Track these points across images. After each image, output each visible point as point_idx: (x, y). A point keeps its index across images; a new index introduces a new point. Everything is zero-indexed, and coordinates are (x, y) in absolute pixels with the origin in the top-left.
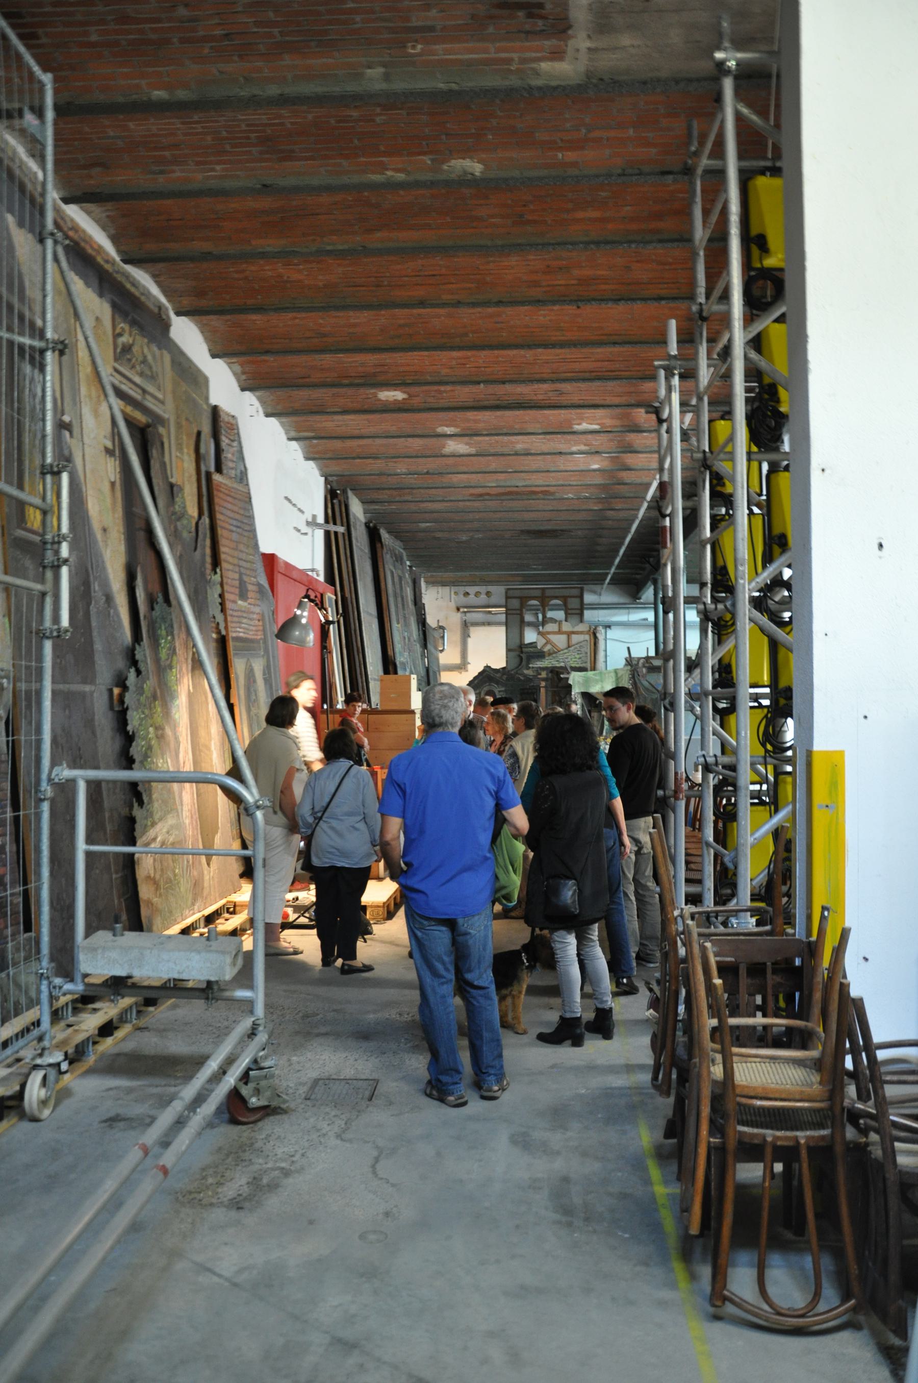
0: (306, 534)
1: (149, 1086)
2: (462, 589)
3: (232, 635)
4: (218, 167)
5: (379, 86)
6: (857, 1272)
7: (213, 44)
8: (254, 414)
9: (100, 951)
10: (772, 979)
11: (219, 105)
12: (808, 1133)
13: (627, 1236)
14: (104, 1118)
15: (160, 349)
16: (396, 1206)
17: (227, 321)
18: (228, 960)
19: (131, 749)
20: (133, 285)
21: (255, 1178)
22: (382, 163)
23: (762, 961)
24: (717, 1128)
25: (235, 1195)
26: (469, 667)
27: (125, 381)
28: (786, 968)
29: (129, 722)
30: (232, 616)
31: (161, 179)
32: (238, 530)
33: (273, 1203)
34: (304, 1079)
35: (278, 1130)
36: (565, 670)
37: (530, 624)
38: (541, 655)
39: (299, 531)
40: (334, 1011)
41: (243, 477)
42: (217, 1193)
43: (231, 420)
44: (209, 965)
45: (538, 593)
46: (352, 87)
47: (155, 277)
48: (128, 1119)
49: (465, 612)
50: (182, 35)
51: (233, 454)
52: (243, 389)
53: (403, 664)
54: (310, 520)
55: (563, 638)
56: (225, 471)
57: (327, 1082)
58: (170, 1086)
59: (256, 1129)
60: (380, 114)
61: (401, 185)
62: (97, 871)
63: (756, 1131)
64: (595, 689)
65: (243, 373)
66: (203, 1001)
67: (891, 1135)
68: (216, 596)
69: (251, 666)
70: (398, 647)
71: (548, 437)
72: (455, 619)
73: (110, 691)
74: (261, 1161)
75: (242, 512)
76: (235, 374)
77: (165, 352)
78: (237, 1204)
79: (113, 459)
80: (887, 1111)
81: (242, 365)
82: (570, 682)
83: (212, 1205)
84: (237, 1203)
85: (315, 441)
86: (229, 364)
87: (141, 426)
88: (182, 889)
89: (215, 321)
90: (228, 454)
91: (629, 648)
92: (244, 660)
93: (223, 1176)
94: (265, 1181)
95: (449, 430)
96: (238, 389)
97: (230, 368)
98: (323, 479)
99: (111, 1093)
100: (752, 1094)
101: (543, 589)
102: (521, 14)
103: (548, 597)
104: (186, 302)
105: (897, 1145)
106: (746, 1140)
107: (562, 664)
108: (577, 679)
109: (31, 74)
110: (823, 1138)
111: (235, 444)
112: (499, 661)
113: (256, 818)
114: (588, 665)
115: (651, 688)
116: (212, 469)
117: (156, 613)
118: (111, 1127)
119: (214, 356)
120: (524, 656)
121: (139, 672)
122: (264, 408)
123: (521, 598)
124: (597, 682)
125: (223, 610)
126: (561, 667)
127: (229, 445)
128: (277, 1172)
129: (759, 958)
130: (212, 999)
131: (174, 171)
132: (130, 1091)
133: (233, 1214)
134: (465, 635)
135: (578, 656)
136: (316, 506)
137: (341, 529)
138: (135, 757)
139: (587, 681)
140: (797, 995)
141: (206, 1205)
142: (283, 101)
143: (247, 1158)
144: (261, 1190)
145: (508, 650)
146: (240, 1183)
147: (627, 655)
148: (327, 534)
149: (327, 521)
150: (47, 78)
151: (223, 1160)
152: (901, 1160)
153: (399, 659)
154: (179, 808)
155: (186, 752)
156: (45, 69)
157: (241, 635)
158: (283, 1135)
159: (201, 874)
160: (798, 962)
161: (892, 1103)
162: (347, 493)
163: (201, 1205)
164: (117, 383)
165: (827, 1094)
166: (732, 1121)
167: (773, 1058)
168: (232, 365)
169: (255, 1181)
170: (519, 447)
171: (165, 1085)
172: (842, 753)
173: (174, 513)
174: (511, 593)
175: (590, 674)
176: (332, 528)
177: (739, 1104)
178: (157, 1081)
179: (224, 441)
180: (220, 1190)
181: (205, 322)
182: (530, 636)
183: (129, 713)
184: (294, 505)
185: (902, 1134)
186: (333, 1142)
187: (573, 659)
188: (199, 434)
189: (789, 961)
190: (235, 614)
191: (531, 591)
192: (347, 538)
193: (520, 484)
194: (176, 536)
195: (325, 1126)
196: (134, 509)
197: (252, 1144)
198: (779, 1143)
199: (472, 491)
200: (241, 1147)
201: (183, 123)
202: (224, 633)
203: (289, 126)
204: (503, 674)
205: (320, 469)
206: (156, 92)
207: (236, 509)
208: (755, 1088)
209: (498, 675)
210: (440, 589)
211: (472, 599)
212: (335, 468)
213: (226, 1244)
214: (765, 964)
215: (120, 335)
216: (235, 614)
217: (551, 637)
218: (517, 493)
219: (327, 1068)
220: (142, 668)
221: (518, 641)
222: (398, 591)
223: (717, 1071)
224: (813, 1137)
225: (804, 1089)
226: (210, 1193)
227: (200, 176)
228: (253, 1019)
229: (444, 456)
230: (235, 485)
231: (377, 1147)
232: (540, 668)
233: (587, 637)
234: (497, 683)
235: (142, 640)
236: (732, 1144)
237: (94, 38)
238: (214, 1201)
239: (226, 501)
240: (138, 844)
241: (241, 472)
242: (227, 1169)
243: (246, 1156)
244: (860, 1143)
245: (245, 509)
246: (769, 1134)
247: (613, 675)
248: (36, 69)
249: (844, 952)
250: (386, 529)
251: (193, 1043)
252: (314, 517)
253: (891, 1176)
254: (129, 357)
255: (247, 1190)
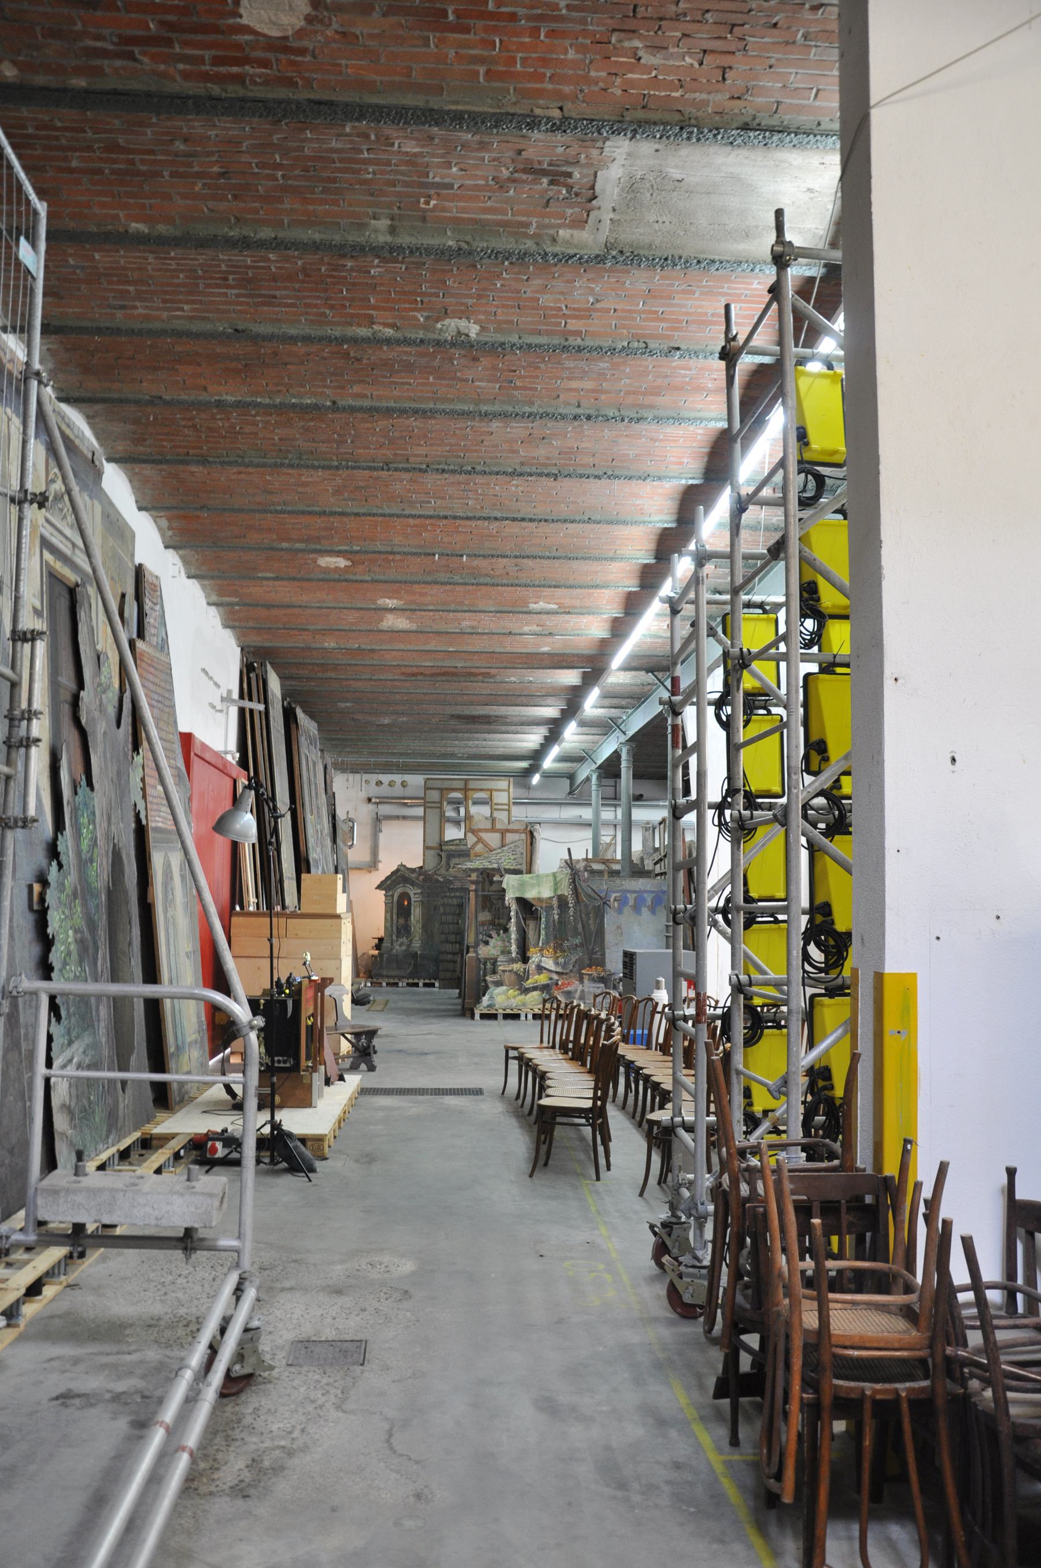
0: (221, 711)
1: (101, 1353)
2: (374, 778)
3: (152, 825)
4: (186, 307)
5: (384, 238)
6: (963, 1539)
7: (208, 181)
8: (176, 574)
9: (62, 1194)
10: (846, 1218)
11: (202, 243)
12: (908, 1385)
13: (692, 1510)
14: (54, 1395)
15: (91, 498)
16: (427, 1486)
17: (161, 470)
18: (217, 1203)
19: (51, 955)
20: (68, 426)
21: (253, 1460)
22: (371, 316)
23: (836, 1199)
24: (808, 1384)
25: (236, 1482)
26: (380, 865)
27: (55, 533)
28: (856, 1204)
29: (49, 923)
30: (151, 803)
31: (119, 314)
32: (160, 705)
33: (282, 1487)
34: (280, 1342)
35: (266, 1403)
36: (500, 872)
37: (449, 820)
38: (465, 854)
39: (214, 707)
40: (294, 1261)
41: (164, 646)
42: (213, 1480)
43: (155, 581)
44: (193, 1209)
45: (460, 785)
46: (353, 238)
47: (90, 418)
48: (84, 1395)
49: (377, 803)
50: (174, 169)
51: (155, 620)
52: (166, 547)
53: (316, 861)
54: (225, 695)
55: (497, 836)
56: (147, 639)
57: (307, 1344)
58: (124, 1353)
59: (240, 1402)
60: (378, 266)
61: (388, 341)
62: (11, 1098)
63: (852, 1384)
64: (530, 895)
65: (170, 528)
66: (180, 1251)
67: (1003, 1384)
68: (138, 780)
69: (169, 860)
70: (311, 842)
71: (498, 615)
72: (364, 813)
73: (30, 888)
74: (254, 1439)
75: (163, 684)
76: (160, 529)
77: (96, 503)
78: (241, 1491)
79: (40, 621)
80: (998, 1358)
81: (169, 519)
82: (504, 886)
83: (211, 1493)
84: (241, 1490)
85: (237, 608)
86: (155, 519)
87: (72, 585)
88: (97, 1119)
89: (148, 470)
90: (150, 620)
91: (569, 850)
92: (163, 854)
93: (215, 1460)
94: (267, 1463)
95: (390, 603)
96: (162, 546)
97: (155, 522)
98: (239, 649)
99: (54, 1364)
100: (847, 1344)
101: (466, 780)
102: (545, 181)
103: (472, 790)
104: (121, 447)
105: (1010, 1395)
106: (843, 1395)
107: (495, 866)
108: (511, 882)
109: (28, 202)
110: (922, 1390)
111: (158, 608)
112: (414, 860)
113: (249, 1039)
114: (524, 868)
115: (593, 894)
116: (135, 636)
117: (79, 799)
118: (65, 1405)
119: (140, 509)
120: (443, 854)
121: (60, 866)
122: (185, 569)
123: (441, 790)
124: (533, 886)
125: (144, 797)
126: (493, 869)
127: (152, 609)
128: (278, 1452)
129: (833, 1196)
130: (192, 1249)
131: (136, 308)
132: (76, 1361)
133: (240, 1503)
134: (376, 831)
135: (512, 857)
136: (232, 682)
137: (261, 707)
138: (54, 964)
139: (522, 885)
140: (868, 1235)
141: (205, 1495)
142: (277, 244)
143: (238, 1437)
144: (265, 1474)
145: (426, 848)
146: (237, 1467)
147: (567, 857)
148: (242, 711)
149: (241, 696)
150: (42, 208)
151: (211, 1440)
152: (1013, 1410)
153: (313, 856)
154: (96, 1023)
155: (104, 958)
156: (41, 198)
157: (160, 824)
158: (273, 1409)
159: (116, 1102)
160: (869, 1199)
161: (1001, 1348)
162: (266, 666)
163: (199, 1494)
164: (47, 535)
165: (927, 1342)
166: (828, 1373)
167: (869, 1305)
168: (158, 520)
169: (254, 1464)
170: (465, 624)
171: (118, 1353)
172: (914, 975)
173: (100, 685)
174: (430, 784)
175: (526, 877)
176: (248, 705)
177: (834, 1355)
178: (107, 1348)
179: (148, 605)
180: (216, 1476)
181: (137, 470)
182: (452, 833)
183: (50, 913)
184: (211, 678)
185: (1014, 1383)
186: (334, 1414)
187: (507, 860)
188: (123, 596)
189: (860, 1199)
190: (155, 801)
191: (446, 782)
192: (263, 717)
193: (459, 665)
194: (101, 711)
195: (319, 1396)
196: (60, 678)
197: (239, 1421)
198: (878, 1397)
199: (403, 670)
200: (227, 1424)
201: (155, 258)
202: (144, 822)
203: (274, 270)
204: (420, 874)
205: (238, 639)
206: (133, 225)
207: (157, 681)
208: (851, 1337)
209: (414, 876)
210: (351, 776)
211: (384, 791)
212: (255, 640)
213: (240, 1540)
214: (839, 1202)
215: (53, 481)
216: (155, 801)
217: (483, 835)
218: (454, 674)
219: (303, 1329)
220: (64, 862)
221: (437, 839)
222: (312, 778)
223: (810, 1319)
224: (913, 1389)
225: (902, 1336)
226: (205, 1480)
227: (165, 315)
228: (239, 1272)
229: (382, 631)
230: (158, 655)
231: (387, 1419)
232: (470, 869)
233: (523, 836)
234: (413, 884)
235: (65, 829)
236: (827, 1400)
237: (74, 164)
238: (213, 1489)
239: (148, 672)
240: (54, 1066)
241: (162, 639)
242: (218, 1450)
243: (237, 1434)
244: (959, 1394)
245: (166, 681)
246: (869, 1387)
247: (551, 878)
248: (33, 197)
249: (942, 1188)
250: (302, 707)
251: (138, 1302)
252: (229, 692)
253: (1004, 1430)
254: (60, 506)
255: (248, 1474)
